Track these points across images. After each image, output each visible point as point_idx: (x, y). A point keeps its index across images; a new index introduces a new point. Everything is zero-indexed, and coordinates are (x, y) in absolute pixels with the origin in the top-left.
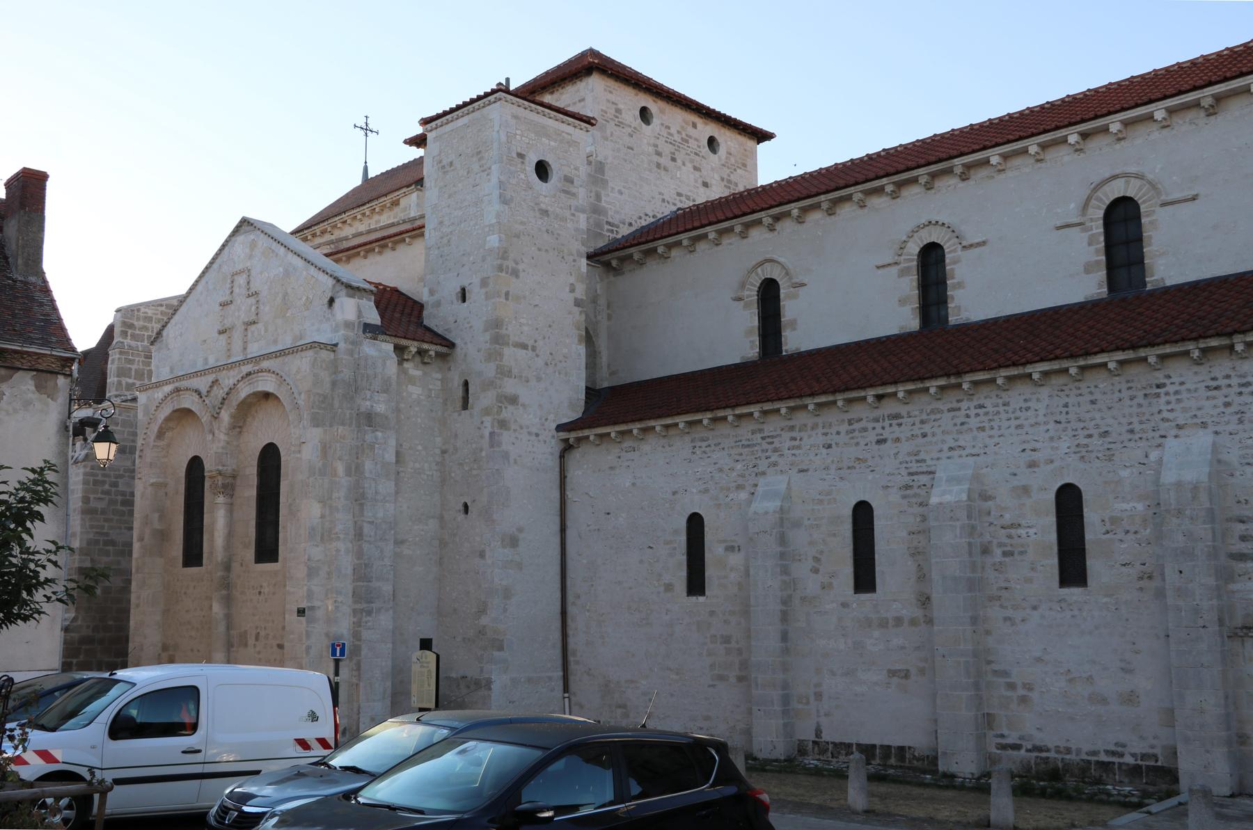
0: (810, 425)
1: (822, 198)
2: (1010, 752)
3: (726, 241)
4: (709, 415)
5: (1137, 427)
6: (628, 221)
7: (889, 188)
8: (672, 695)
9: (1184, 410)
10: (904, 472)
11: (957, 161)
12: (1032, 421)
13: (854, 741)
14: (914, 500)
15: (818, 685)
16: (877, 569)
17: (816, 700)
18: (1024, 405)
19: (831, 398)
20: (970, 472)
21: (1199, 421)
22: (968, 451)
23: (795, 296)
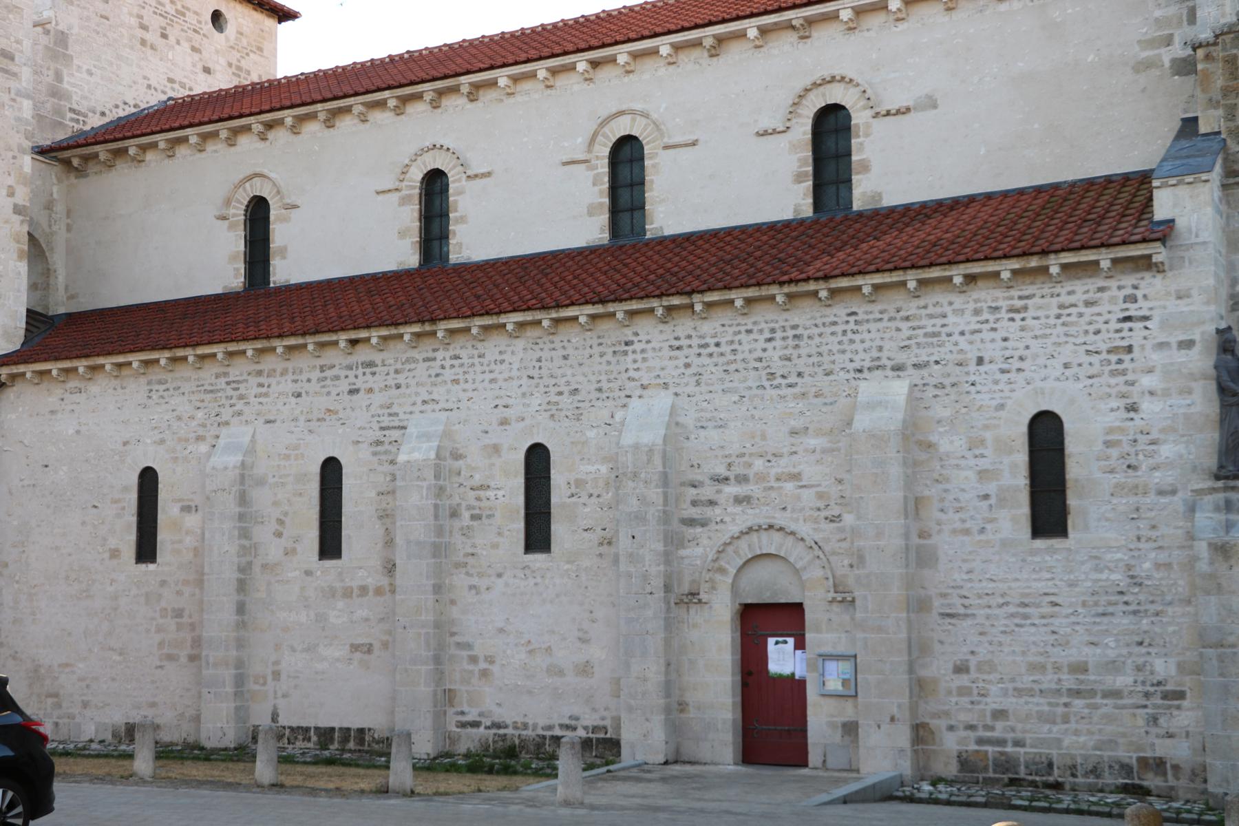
0: (279, 371)
1: (319, 107)
2: (469, 730)
3: (211, 147)
4: (167, 354)
5: (605, 385)
6: (99, 109)
7: (392, 103)
8: (113, 679)
9: (649, 369)
10: (376, 426)
11: (463, 79)
12: (506, 375)
13: (312, 725)
14: (384, 457)
15: (277, 663)
16: (344, 533)
17: (274, 679)
18: (499, 358)
19: (300, 341)
20: (441, 428)
21: (662, 382)
22: (442, 405)
23: (285, 220)
